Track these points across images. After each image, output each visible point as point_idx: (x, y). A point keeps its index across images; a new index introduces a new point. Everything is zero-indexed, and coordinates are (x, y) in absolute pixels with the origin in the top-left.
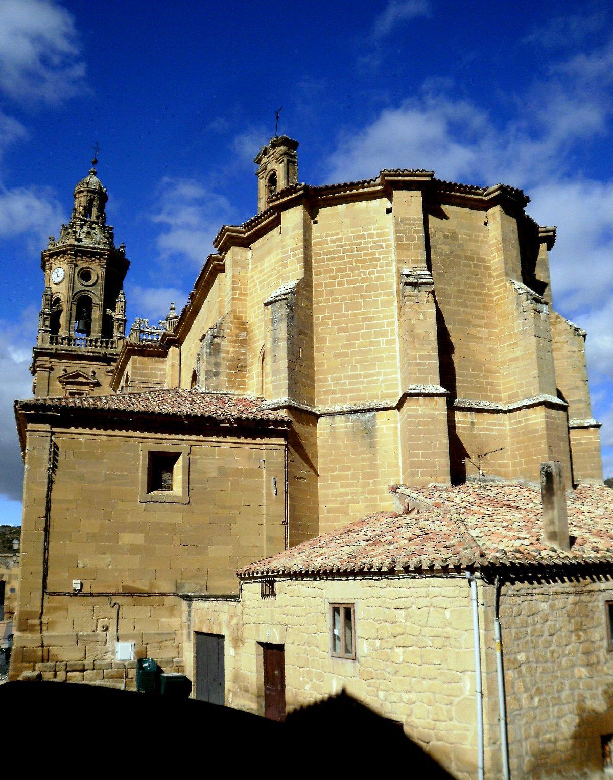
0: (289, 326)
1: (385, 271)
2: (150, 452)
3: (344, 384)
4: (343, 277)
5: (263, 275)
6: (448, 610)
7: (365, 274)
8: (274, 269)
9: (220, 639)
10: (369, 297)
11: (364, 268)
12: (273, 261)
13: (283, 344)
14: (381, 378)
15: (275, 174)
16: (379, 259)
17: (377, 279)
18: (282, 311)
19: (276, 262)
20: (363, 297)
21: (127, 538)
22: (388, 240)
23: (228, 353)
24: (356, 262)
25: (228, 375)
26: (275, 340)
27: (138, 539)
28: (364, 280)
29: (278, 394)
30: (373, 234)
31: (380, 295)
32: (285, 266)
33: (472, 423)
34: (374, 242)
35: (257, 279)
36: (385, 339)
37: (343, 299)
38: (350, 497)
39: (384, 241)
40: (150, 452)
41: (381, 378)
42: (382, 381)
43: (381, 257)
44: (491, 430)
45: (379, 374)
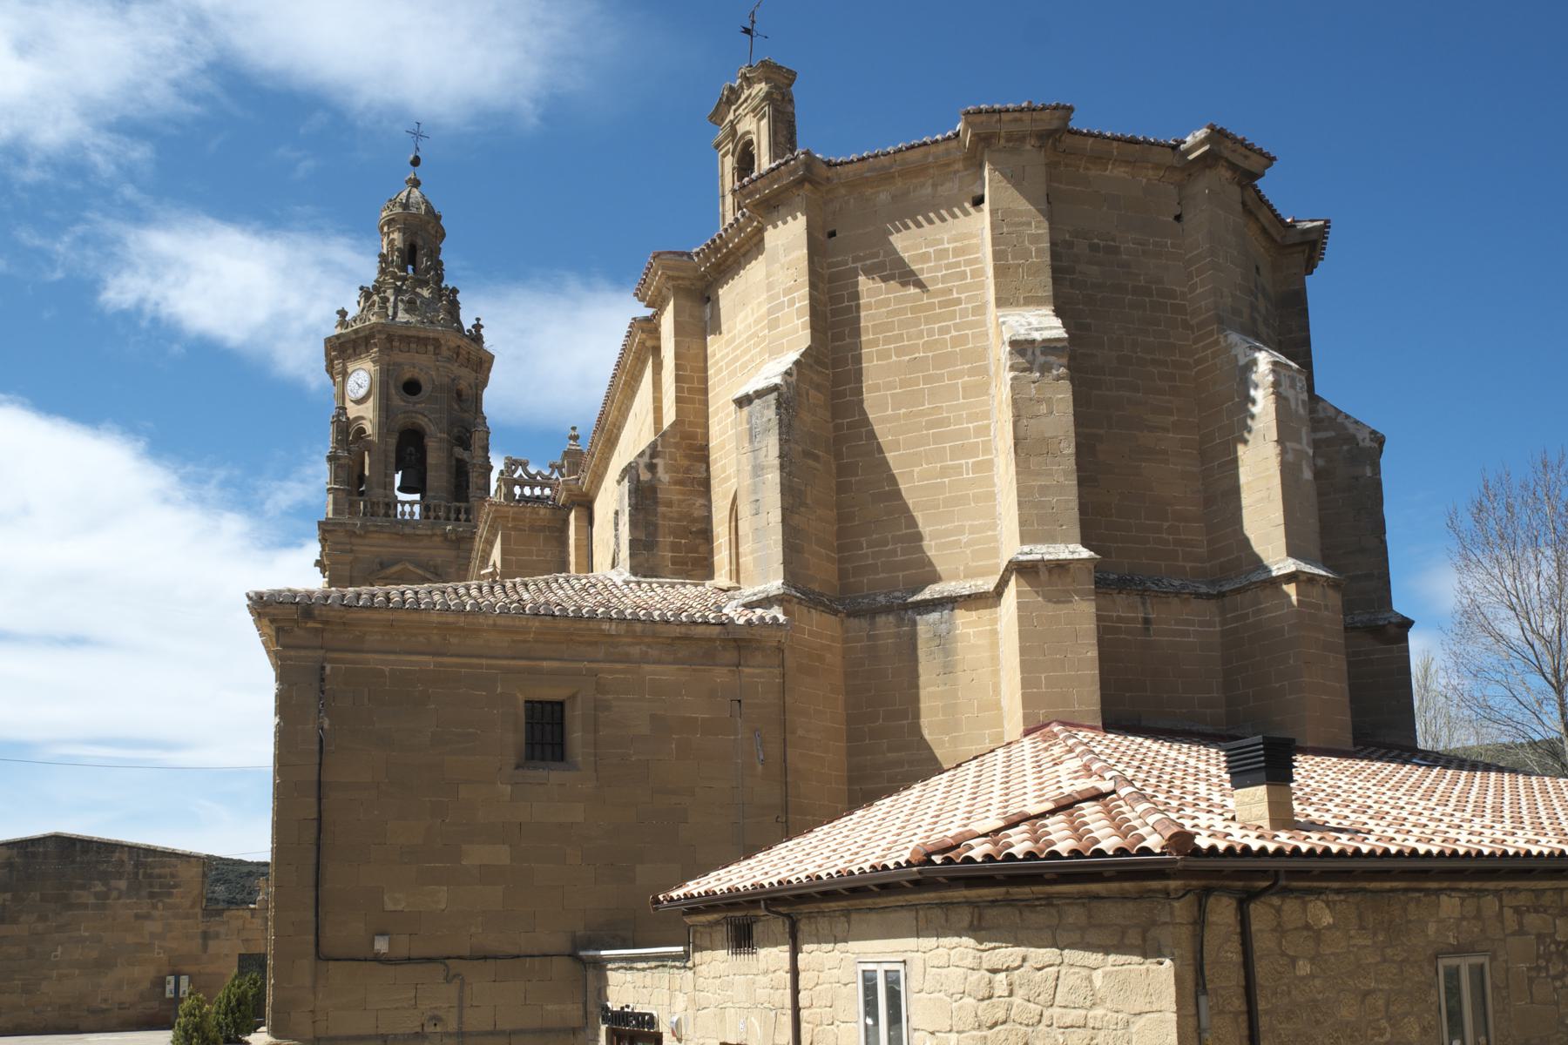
0: (783, 442)
1: (971, 325)
2: (531, 704)
3: (894, 552)
4: (887, 341)
5: (734, 350)
6: (1099, 971)
7: (931, 332)
8: (755, 334)
9: (591, 974)
10: (940, 378)
11: (928, 320)
12: (751, 320)
13: (773, 478)
14: (964, 538)
15: (750, 142)
16: (958, 302)
17: (956, 341)
18: (767, 412)
19: (757, 322)
20: (927, 379)
21: (478, 855)
22: (976, 261)
23: (669, 504)
24: (913, 310)
25: (675, 547)
26: (758, 470)
27: (501, 855)
28: (928, 346)
29: (766, 579)
30: (946, 250)
31: (961, 374)
32: (773, 325)
33: (1146, 621)
34: (948, 267)
35: (723, 358)
36: (971, 461)
37: (889, 386)
38: (906, 768)
39: (968, 263)
40: (531, 704)
41: (964, 538)
42: (968, 544)
43: (963, 296)
44: (1186, 634)
45: (960, 530)
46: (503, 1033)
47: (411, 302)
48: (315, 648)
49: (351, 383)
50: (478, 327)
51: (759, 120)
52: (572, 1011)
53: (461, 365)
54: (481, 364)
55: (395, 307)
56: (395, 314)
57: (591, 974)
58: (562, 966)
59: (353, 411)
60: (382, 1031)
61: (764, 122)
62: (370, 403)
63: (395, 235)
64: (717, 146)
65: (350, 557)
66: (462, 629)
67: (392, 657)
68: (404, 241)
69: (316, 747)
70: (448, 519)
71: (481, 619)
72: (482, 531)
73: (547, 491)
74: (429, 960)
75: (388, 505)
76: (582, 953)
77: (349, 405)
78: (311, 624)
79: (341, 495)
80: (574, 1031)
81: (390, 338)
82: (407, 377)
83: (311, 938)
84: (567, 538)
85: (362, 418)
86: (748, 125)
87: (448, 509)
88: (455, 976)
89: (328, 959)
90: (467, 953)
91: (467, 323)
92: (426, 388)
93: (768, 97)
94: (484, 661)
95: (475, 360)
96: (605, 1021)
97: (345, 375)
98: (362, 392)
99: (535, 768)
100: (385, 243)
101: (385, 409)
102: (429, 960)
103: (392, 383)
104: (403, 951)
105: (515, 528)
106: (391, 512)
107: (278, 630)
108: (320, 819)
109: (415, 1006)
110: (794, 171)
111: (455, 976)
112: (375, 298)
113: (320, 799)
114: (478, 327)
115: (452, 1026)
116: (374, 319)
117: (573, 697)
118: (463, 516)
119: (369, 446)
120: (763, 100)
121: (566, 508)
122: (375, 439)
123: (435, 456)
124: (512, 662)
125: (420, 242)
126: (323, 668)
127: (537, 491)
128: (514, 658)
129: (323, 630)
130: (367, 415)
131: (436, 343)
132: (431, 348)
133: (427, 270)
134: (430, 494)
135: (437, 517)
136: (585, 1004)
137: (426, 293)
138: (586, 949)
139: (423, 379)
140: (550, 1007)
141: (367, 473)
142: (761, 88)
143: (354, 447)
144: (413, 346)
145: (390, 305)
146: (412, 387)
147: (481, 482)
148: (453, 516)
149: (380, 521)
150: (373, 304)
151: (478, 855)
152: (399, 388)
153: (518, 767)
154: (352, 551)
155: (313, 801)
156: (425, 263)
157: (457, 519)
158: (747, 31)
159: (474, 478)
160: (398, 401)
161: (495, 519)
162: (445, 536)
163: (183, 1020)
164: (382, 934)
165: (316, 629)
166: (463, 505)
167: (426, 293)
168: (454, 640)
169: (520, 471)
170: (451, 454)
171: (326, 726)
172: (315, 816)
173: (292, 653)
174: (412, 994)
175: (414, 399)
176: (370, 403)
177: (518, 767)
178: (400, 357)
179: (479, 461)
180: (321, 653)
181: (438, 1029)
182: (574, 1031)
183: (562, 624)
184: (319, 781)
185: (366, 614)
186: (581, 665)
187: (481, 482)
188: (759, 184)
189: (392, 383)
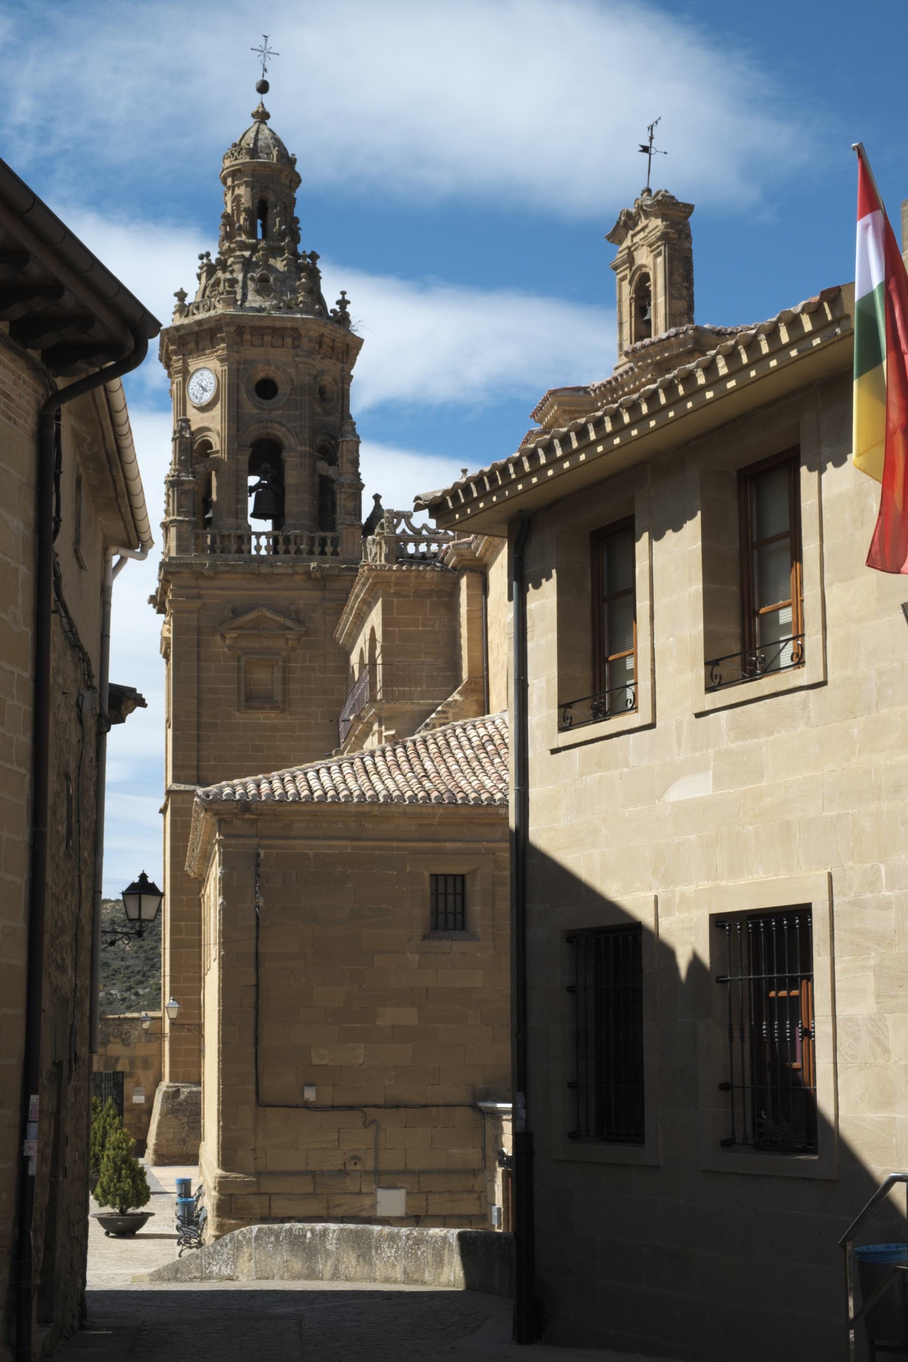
9: (489, 1123)
21: (390, 1016)
27: (409, 1017)
46: (412, 1172)
47: (263, 280)
48: (251, 837)
49: (193, 385)
50: (343, 303)
51: (656, 256)
52: (471, 1155)
53: (325, 356)
54: (350, 348)
55: (245, 287)
56: (245, 296)
57: (489, 1123)
58: (464, 1115)
59: (197, 420)
60: (310, 1168)
61: (660, 260)
62: (217, 411)
63: (241, 191)
64: (615, 268)
65: (197, 604)
66: (376, 816)
67: (316, 843)
68: (253, 198)
69: (254, 923)
70: (311, 552)
71: (393, 809)
72: (359, 591)
73: (434, 547)
74: (350, 1108)
75: (240, 538)
76: (481, 1104)
77: (192, 413)
78: (247, 816)
79: (186, 528)
80: (474, 1172)
81: (240, 330)
82: (261, 376)
83: (252, 1087)
84: (460, 657)
85: (208, 429)
86: (643, 257)
87: (312, 540)
88: (371, 1122)
89: (267, 1106)
90: (381, 1102)
91: (331, 304)
92: (284, 389)
93: (664, 237)
94: (395, 844)
95: (338, 342)
96: (501, 1165)
97: (186, 374)
98: (207, 397)
99: (440, 939)
100: (229, 198)
101: (235, 418)
102: (350, 1108)
103: (242, 386)
104: (328, 1101)
105: (397, 594)
106: (244, 547)
107: (220, 821)
108: (257, 986)
109: (338, 1147)
110: (683, 343)
111: (371, 1122)
112: (219, 274)
113: (257, 969)
114: (343, 303)
115: (370, 1165)
116: (220, 309)
117: (473, 873)
118: (329, 549)
119: (217, 464)
120: (659, 239)
121: (458, 571)
122: (224, 456)
123: (295, 475)
124: (420, 844)
125: (271, 198)
126: (258, 855)
127: (423, 548)
128: (421, 840)
129: (257, 820)
130: (214, 425)
131: (295, 333)
132: (288, 341)
133: (282, 235)
134: (289, 521)
135: (298, 551)
136: (484, 1149)
137: (280, 264)
138: (485, 1100)
139: (279, 378)
140: (453, 1151)
141: (214, 497)
142: (656, 224)
143: (200, 468)
144: (267, 338)
145: (239, 289)
146: (266, 389)
147: (351, 504)
148: (317, 549)
149: (232, 559)
150: (217, 283)
151: (390, 1016)
152: (252, 390)
153: (425, 938)
154: (199, 597)
155: (252, 970)
156: (277, 225)
157: (323, 553)
158: (645, 149)
159: (342, 500)
160: (250, 408)
161: (374, 584)
162: (308, 574)
163: (112, 1153)
164: (310, 1085)
165: (251, 819)
166: (329, 535)
167: (280, 264)
168: (369, 826)
169: (403, 526)
170: (313, 469)
171: (261, 904)
172: (254, 982)
173: (233, 842)
174: (335, 1137)
175: (268, 403)
176: (217, 411)
177: (425, 938)
178: (251, 353)
179: (346, 479)
180: (255, 841)
181: (358, 1167)
182: (474, 1172)
183: (463, 811)
184: (257, 954)
185: (294, 807)
186: (479, 845)
187: (351, 504)
188: (650, 350)
189: (242, 386)
